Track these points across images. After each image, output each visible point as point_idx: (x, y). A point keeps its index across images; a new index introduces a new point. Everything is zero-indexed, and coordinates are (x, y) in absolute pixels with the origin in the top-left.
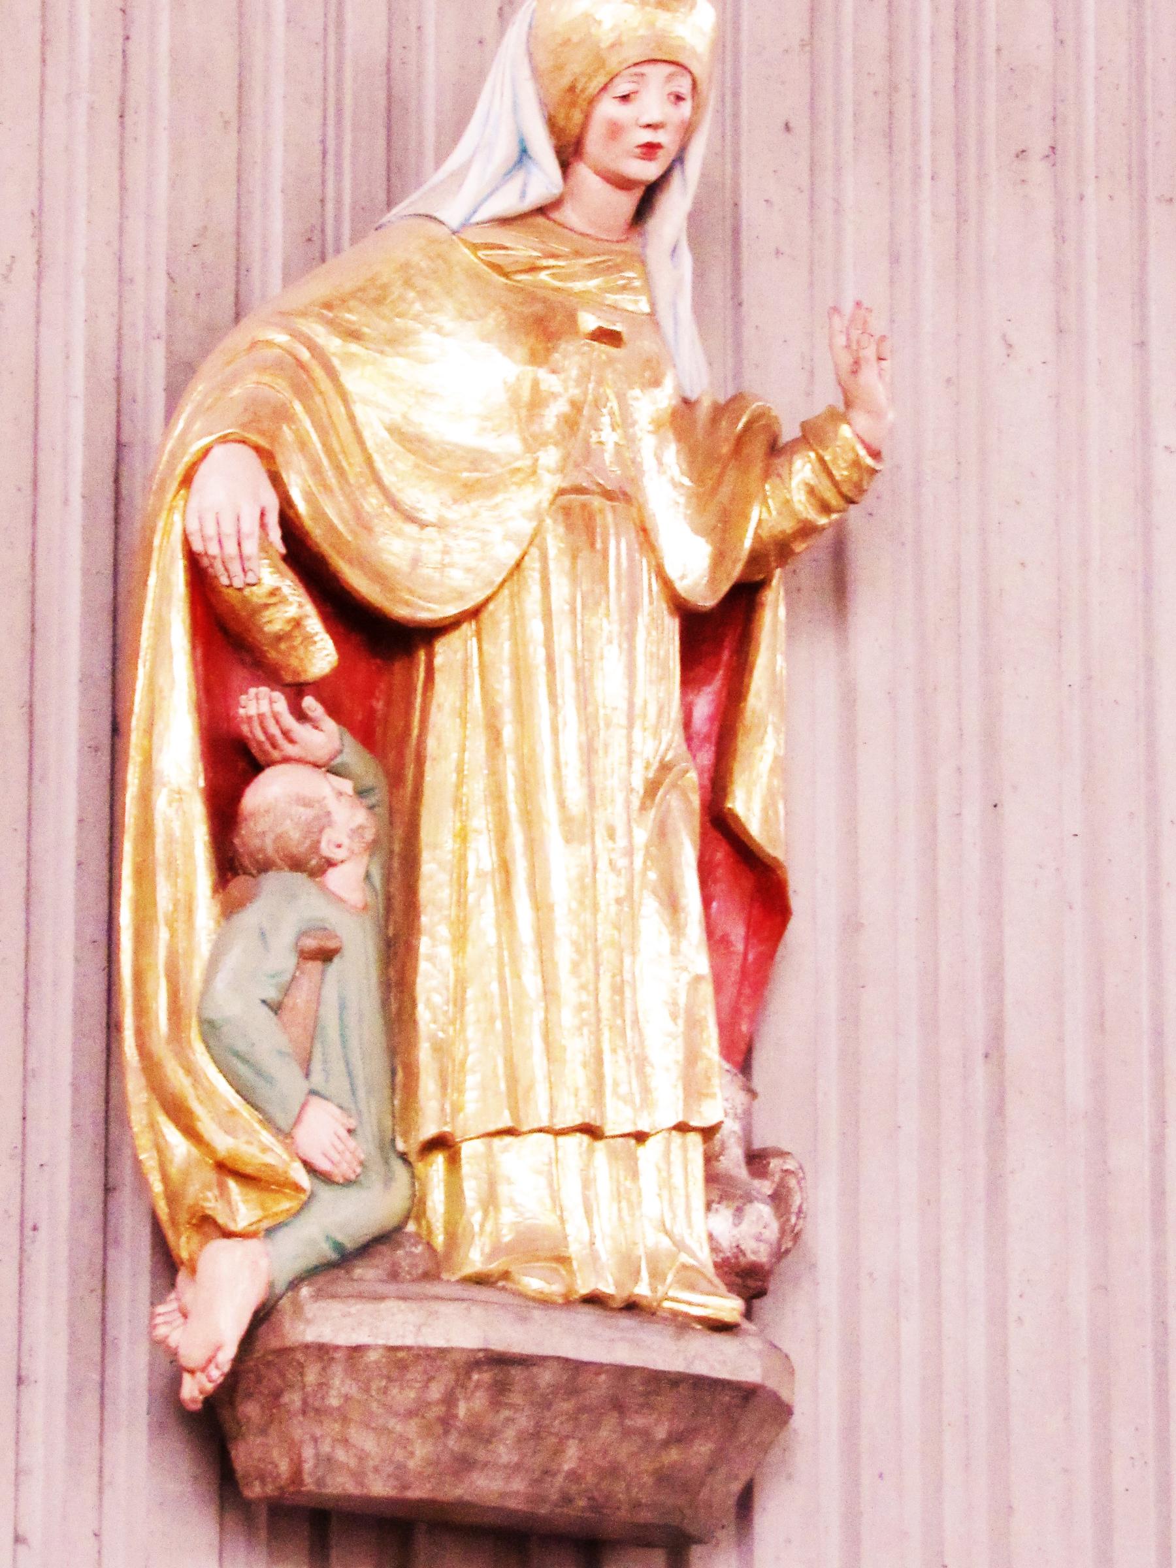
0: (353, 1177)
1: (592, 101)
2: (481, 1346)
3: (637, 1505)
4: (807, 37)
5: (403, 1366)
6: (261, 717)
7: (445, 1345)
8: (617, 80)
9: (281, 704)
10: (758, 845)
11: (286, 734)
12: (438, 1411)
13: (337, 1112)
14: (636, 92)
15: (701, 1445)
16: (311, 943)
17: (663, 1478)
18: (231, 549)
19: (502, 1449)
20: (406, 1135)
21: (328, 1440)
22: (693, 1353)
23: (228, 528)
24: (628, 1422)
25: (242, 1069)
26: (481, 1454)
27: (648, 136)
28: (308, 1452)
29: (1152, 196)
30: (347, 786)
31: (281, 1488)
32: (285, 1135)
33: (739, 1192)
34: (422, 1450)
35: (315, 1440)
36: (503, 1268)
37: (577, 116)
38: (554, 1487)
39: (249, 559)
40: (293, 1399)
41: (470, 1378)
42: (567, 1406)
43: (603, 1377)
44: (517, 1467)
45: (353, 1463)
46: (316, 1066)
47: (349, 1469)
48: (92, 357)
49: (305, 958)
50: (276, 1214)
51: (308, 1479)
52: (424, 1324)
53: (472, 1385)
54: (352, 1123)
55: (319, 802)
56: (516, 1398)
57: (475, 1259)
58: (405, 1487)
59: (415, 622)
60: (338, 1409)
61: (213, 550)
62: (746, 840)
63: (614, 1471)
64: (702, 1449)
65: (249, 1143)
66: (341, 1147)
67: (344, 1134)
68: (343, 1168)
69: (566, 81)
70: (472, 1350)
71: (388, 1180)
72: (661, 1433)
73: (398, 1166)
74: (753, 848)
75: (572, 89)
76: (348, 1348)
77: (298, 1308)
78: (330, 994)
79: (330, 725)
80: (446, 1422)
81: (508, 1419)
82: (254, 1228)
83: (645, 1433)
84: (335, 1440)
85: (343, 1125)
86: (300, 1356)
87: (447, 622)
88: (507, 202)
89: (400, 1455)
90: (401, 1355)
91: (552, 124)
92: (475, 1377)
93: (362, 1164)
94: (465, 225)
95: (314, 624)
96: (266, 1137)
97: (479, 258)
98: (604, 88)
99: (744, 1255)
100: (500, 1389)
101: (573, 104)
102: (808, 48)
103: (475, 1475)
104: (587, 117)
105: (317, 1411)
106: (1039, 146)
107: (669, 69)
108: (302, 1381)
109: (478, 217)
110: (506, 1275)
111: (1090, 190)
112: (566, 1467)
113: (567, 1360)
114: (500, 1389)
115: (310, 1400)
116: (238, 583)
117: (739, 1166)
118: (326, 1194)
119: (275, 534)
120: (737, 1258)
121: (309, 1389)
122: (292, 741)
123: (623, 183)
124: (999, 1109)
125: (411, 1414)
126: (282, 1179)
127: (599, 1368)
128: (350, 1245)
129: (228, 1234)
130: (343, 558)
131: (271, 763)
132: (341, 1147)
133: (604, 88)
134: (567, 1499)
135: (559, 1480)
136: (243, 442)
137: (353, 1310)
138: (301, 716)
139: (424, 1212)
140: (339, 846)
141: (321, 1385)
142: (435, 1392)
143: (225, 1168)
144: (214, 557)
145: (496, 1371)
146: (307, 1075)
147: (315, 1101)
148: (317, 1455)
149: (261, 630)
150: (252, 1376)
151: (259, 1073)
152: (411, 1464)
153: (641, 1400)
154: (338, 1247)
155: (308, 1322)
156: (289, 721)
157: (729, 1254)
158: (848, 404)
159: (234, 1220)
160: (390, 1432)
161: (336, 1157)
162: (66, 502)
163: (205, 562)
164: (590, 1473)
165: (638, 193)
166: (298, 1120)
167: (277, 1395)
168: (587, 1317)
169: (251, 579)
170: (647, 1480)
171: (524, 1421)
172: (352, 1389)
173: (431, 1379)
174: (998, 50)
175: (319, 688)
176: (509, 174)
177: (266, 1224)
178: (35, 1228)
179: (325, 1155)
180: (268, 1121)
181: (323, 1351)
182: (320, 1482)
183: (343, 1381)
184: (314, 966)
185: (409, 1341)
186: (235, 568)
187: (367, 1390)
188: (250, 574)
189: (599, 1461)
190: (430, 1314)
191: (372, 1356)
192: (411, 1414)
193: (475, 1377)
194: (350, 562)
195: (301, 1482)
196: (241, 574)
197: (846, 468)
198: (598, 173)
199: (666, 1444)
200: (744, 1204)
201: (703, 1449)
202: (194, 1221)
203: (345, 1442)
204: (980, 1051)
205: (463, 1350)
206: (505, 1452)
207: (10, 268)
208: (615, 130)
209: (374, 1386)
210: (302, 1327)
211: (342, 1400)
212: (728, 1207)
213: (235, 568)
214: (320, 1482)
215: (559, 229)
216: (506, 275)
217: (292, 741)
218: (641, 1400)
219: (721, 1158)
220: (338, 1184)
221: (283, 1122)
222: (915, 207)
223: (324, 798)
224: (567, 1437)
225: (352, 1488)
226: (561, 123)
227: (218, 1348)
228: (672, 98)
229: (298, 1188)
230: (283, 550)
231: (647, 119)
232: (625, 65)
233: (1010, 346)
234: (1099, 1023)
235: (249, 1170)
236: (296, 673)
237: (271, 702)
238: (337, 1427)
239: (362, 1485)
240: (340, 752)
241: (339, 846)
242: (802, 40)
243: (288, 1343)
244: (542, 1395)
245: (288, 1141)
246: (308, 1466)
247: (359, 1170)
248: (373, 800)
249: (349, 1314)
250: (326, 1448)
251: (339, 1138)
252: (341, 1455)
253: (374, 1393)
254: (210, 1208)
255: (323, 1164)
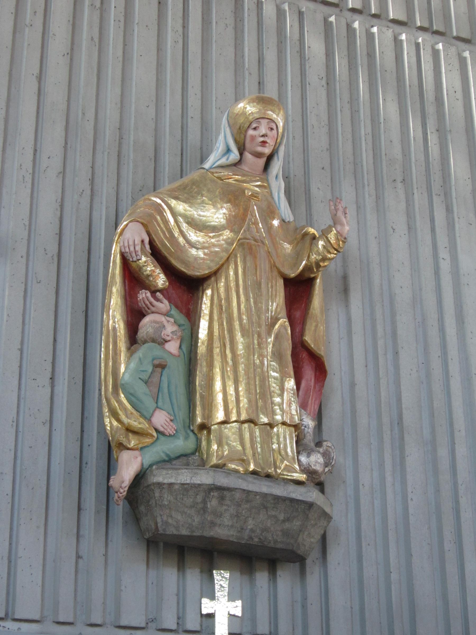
0: (173, 434)
1: (246, 131)
2: (212, 483)
3: (276, 542)
4: (328, 148)
5: (187, 490)
6: (143, 298)
7: (201, 483)
8: (252, 124)
9: (149, 294)
10: (315, 351)
11: (151, 303)
12: (201, 506)
13: (167, 414)
14: (258, 127)
15: (296, 522)
16: (156, 362)
17: (286, 533)
18: (132, 249)
19: (225, 520)
20: (193, 425)
21: (165, 516)
22: (290, 491)
23: (131, 243)
24: (269, 513)
25: (133, 399)
26: (218, 521)
27: (262, 139)
28: (159, 520)
29: (434, 194)
30: (172, 320)
31: (153, 533)
32: (149, 420)
33: (309, 448)
34: (197, 519)
35: (161, 516)
36: (223, 463)
37: (242, 136)
38: (246, 535)
39: (137, 251)
40: (152, 502)
41: (210, 494)
42: (247, 506)
43: (258, 497)
44: (232, 526)
45: (175, 523)
46: (160, 400)
47: (174, 526)
48: (107, 219)
49: (155, 367)
50: (143, 443)
51: (160, 529)
52: (193, 476)
53: (211, 497)
54: (172, 418)
55: (161, 322)
56: (228, 502)
57: (214, 461)
58: (193, 532)
59: (195, 276)
60: (168, 505)
61: (127, 250)
62: (310, 348)
63: (265, 530)
64: (297, 523)
65: (135, 421)
66: (167, 424)
67: (168, 420)
68: (170, 431)
69: (238, 127)
70: (209, 485)
71: (187, 438)
72: (281, 517)
73: (191, 434)
74: (313, 351)
75: (240, 128)
76: (168, 484)
77: (152, 471)
78: (164, 379)
79: (166, 302)
80: (204, 509)
81: (226, 510)
82: (136, 446)
83: (275, 517)
84: (167, 516)
85: (169, 418)
86: (153, 487)
87: (205, 276)
88: (223, 161)
89: (190, 521)
90: (186, 486)
91: (236, 141)
92: (212, 494)
93: (176, 431)
94: (211, 168)
95: (158, 271)
96: (141, 420)
97: (215, 176)
98: (249, 127)
99: (311, 467)
100: (222, 498)
101: (241, 133)
102: (329, 151)
103: (217, 528)
104: (245, 136)
105: (160, 505)
106: (399, 179)
107: (267, 121)
108: (154, 496)
109: (214, 166)
110: (224, 465)
111: (415, 191)
112: (249, 527)
113: (244, 490)
114: (222, 498)
115: (158, 502)
116: (135, 259)
117: (310, 442)
118: (162, 438)
119: (148, 247)
120: (309, 467)
121: (156, 498)
122: (153, 306)
123: (258, 155)
124: (402, 438)
125: (192, 507)
126: (146, 432)
127: (256, 493)
128: (172, 456)
129: (128, 449)
130: (172, 257)
131: (149, 314)
132: (167, 424)
133: (249, 127)
134: (251, 538)
135: (248, 531)
136: (138, 221)
137: (170, 472)
138: (158, 300)
139: (201, 449)
140: (168, 336)
141: (160, 497)
142: (199, 499)
143: (129, 430)
144: (127, 252)
145: (219, 492)
146: (157, 403)
147: (158, 410)
148: (162, 521)
149: (143, 274)
150: (141, 497)
151: (138, 400)
152: (194, 524)
153: (273, 505)
154: (167, 455)
155: (154, 476)
156: (152, 300)
157: (306, 466)
158: (335, 224)
159: (130, 445)
160: (186, 513)
161: (165, 427)
162: (100, 258)
163: (125, 255)
164: (258, 530)
165: (264, 159)
166: (152, 415)
167: (149, 501)
168: (250, 478)
169: (138, 258)
170: (280, 533)
171: (232, 510)
172: (171, 498)
173: (197, 494)
174: (386, 154)
175: (161, 291)
176: (224, 155)
177: (140, 446)
178: (86, 463)
179: (162, 426)
180: (142, 415)
181: (160, 485)
182: (164, 530)
183: (168, 495)
184: (159, 370)
185: (188, 482)
186: (134, 255)
187: (176, 499)
188: (138, 256)
189: (260, 526)
190: (195, 473)
191: (177, 487)
192: (192, 507)
193: (212, 494)
194: (175, 259)
195: (158, 531)
196: (135, 257)
197: (334, 240)
198: (251, 154)
199: (284, 521)
200: (311, 452)
201: (297, 524)
202: (117, 445)
203: (171, 516)
204: (396, 423)
205: (206, 485)
206: (227, 520)
207: (82, 193)
208: (253, 138)
209: (179, 497)
210: (153, 478)
211: (168, 502)
212: (305, 452)
213: (134, 255)
214: (164, 530)
215: (240, 170)
216: (222, 180)
217: (153, 306)
218: (273, 505)
219: (304, 439)
220: (166, 435)
221: (148, 417)
222: (364, 194)
223: (163, 322)
224: (248, 517)
225: (175, 532)
226: (238, 139)
227: (123, 482)
228: (270, 129)
229: (152, 436)
230: (150, 251)
231: (261, 134)
232: (254, 119)
233: (394, 229)
234: (432, 415)
235: (135, 430)
236: (155, 287)
237: (146, 294)
238: (168, 511)
239: (179, 531)
240: (170, 311)
241: (168, 336)
242: (327, 148)
243: (149, 483)
244: (237, 502)
245: (149, 422)
246: (159, 525)
247: (175, 432)
248: (183, 328)
249: (168, 474)
250: (165, 518)
251: (167, 421)
252: (170, 521)
253: (178, 499)
254: (121, 440)
255: (161, 429)
